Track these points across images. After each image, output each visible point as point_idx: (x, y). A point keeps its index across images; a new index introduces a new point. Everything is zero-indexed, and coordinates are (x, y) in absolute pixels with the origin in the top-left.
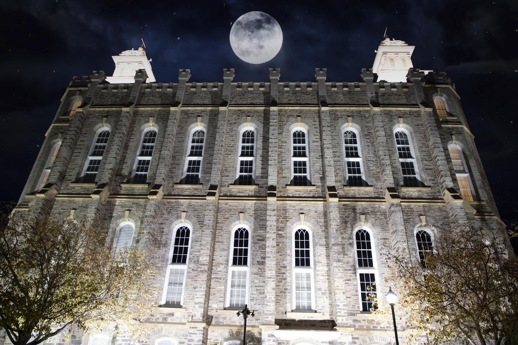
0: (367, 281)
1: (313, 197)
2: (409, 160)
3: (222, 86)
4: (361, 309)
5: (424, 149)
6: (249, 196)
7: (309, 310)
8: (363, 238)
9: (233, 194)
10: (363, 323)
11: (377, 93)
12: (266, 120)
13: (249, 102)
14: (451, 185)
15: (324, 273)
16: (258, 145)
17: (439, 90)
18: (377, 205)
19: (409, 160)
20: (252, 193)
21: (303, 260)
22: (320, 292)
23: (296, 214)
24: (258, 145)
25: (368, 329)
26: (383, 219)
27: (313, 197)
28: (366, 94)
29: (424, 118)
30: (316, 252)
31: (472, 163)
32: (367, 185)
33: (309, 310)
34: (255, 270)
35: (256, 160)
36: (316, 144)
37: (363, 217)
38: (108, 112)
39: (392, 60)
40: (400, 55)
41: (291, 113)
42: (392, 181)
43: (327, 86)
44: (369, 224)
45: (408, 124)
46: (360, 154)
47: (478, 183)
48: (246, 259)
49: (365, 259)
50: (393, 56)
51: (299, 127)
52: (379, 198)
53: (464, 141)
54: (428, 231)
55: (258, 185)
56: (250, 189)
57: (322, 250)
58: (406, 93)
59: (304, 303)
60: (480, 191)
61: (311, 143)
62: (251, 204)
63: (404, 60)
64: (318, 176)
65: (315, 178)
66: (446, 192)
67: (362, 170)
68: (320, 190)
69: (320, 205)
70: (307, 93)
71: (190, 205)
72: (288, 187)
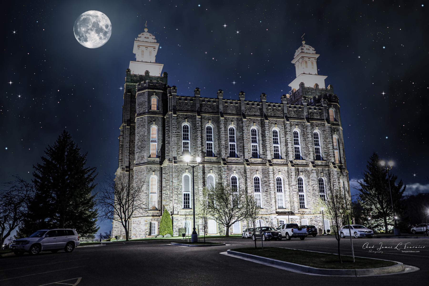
0: (301, 198)
1: (283, 164)
2: (318, 147)
3: (240, 103)
4: (183, 207)
5: (325, 143)
6: (259, 163)
7: (282, 208)
8: (300, 182)
9: (253, 162)
10: (301, 212)
11: (308, 112)
12: (262, 125)
13: (253, 113)
14: (333, 161)
15: (288, 195)
16: (259, 138)
17: (332, 106)
18: (306, 168)
19: (318, 147)
20: (260, 162)
21: (279, 190)
22: (287, 202)
23: (277, 171)
24: (259, 138)
25: (303, 214)
26: (308, 174)
27: (283, 164)
28: (303, 113)
29: (327, 128)
30: (285, 187)
31: (341, 146)
32: (303, 159)
33: (282, 208)
34: (265, 194)
35: (259, 146)
36: (283, 139)
37: (301, 173)
38: (186, 115)
39: (306, 62)
40: (311, 59)
41: (272, 122)
42: (313, 159)
43: (287, 106)
44: (303, 176)
45: (319, 130)
46: (300, 143)
47: (342, 156)
48: (259, 189)
49: (301, 189)
50: (306, 59)
51: (276, 129)
52: (307, 165)
53: (339, 135)
54: (323, 178)
55: (262, 158)
56: (259, 160)
57: (287, 186)
58: (320, 112)
59: (280, 205)
60: (342, 159)
61: (281, 139)
62: (260, 167)
63: (312, 63)
64: (285, 154)
65: (284, 156)
66: (331, 163)
67: (300, 151)
68: (285, 161)
69: (286, 168)
70: (278, 110)
71: (236, 167)
72: (274, 160)
